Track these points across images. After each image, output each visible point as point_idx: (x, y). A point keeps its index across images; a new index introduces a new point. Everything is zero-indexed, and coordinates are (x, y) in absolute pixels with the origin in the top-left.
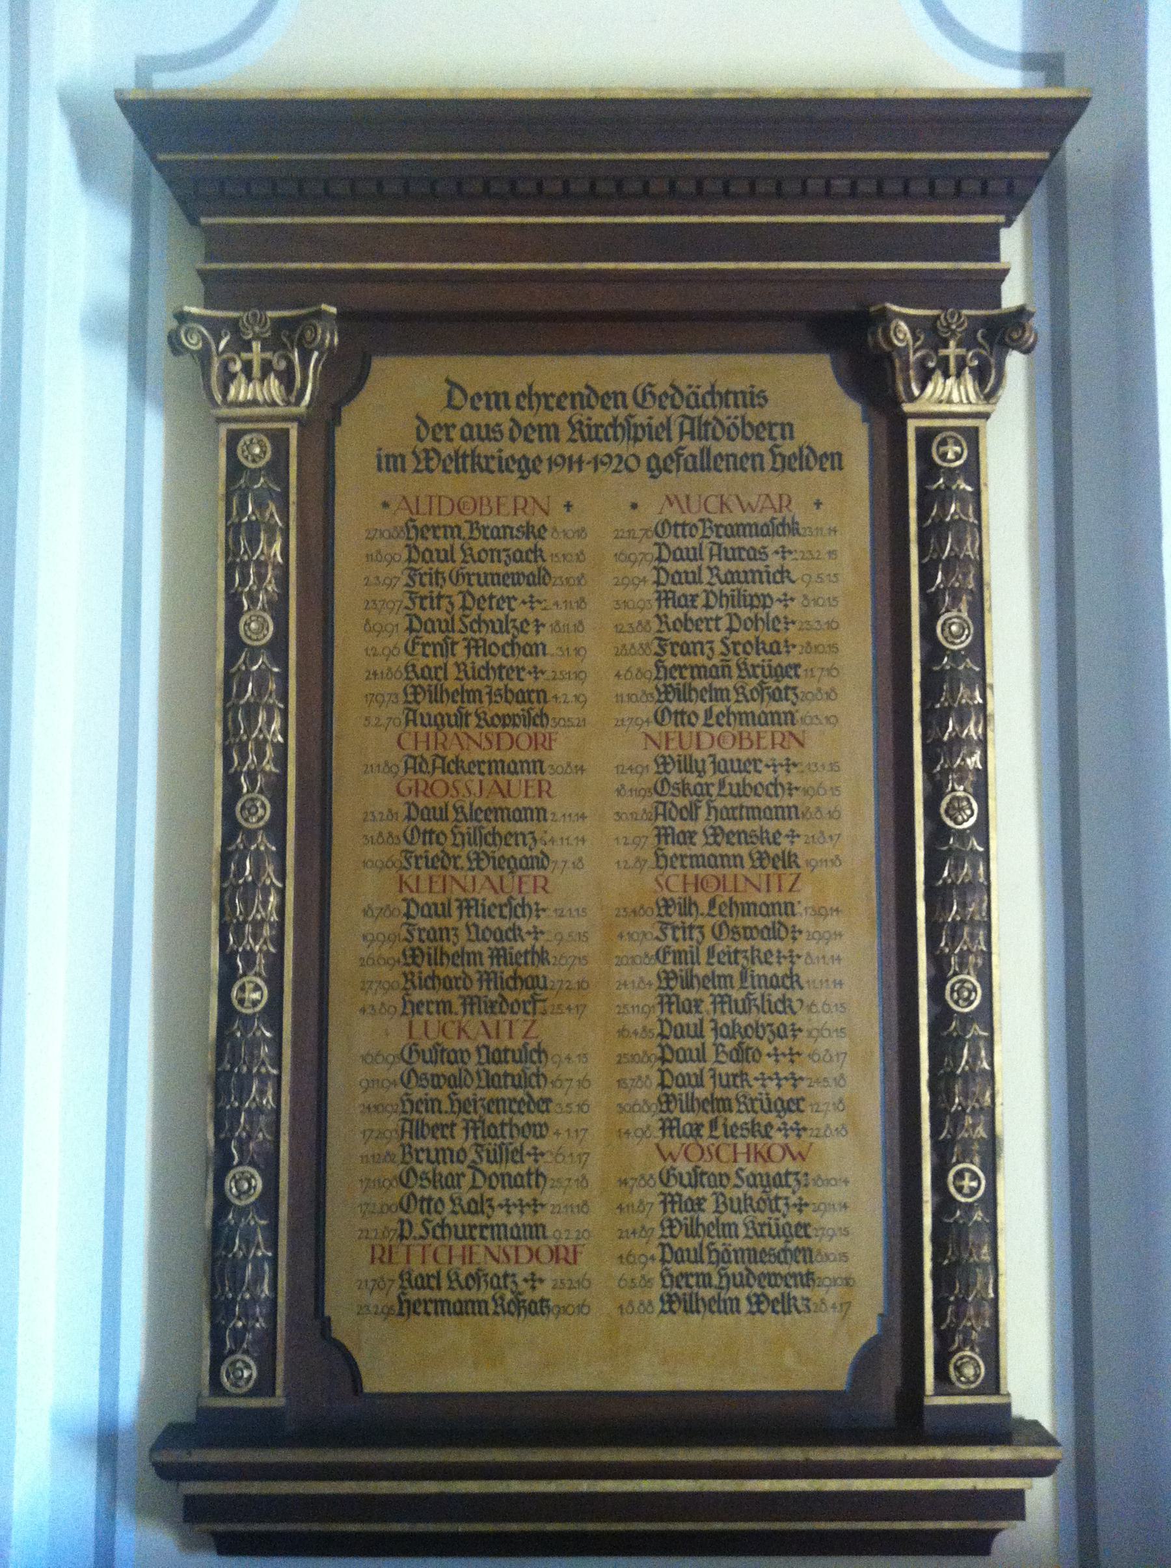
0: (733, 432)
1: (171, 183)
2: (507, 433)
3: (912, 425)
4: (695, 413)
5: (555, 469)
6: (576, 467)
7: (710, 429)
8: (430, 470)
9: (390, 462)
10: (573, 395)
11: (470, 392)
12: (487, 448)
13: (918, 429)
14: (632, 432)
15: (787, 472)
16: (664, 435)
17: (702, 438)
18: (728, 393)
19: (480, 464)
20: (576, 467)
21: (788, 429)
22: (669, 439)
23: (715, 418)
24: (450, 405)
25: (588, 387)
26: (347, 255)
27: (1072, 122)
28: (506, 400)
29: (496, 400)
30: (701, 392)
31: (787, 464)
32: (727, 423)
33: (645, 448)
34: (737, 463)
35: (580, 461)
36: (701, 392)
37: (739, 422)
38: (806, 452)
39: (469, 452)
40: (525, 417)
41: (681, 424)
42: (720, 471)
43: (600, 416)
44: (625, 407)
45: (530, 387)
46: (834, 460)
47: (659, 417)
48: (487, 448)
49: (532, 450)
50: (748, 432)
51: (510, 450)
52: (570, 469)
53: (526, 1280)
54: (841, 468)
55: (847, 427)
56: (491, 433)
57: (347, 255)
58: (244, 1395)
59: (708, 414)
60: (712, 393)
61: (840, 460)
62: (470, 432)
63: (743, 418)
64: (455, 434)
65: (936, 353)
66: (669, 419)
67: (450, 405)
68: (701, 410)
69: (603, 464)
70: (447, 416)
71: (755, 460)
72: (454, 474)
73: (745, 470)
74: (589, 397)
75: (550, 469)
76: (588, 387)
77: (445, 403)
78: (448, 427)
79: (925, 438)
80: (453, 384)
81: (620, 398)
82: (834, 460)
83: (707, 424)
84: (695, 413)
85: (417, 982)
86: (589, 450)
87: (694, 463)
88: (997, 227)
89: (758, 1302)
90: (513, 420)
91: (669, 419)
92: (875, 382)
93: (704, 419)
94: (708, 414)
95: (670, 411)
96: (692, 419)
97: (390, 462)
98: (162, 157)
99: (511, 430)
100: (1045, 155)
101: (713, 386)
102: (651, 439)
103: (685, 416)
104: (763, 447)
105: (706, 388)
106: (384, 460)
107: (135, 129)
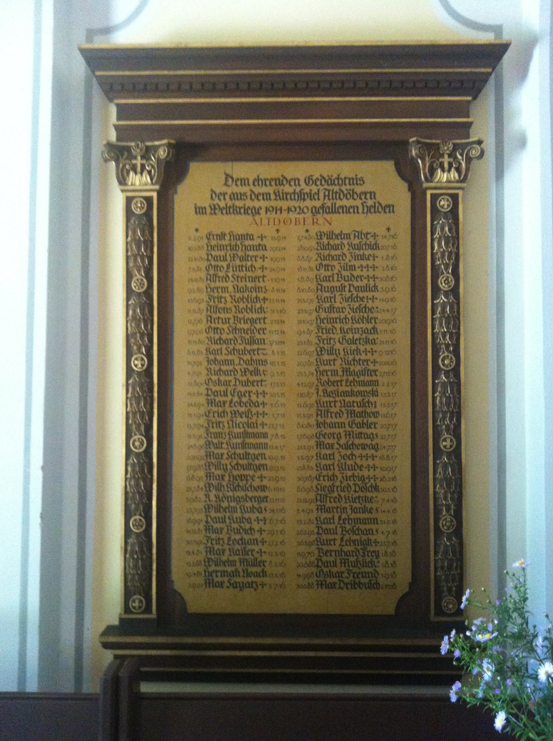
0: (348, 196)
1: (101, 84)
2: (249, 197)
3: (429, 193)
4: (330, 188)
5: (269, 213)
6: (279, 212)
7: (338, 195)
8: (215, 213)
9: (200, 211)
10: (275, 179)
11: (235, 178)
12: (239, 203)
13: (431, 194)
14: (301, 196)
15: (369, 214)
16: (316, 197)
17: (336, 197)
18: (345, 178)
19: (236, 211)
20: (279, 212)
21: (373, 195)
22: (319, 199)
23: (340, 190)
24: (226, 184)
25: (282, 176)
26: (182, 120)
27: (506, 50)
28: (248, 182)
29: (244, 182)
30: (333, 178)
31: (369, 210)
32: (345, 192)
33: (309, 203)
34: (347, 210)
35: (281, 210)
36: (333, 178)
37: (351, 192)
38: (377, 205)
39: (232, 205)
40: (257, 190)
41: (325, 193)
42: (350, 213)
43: (288, 189)
44: (299, 185)
45: (258, 177)
46: (389, 208)
47: (314, 189)
48: (239, 203)
49: (257, 204)
50: (355, 196)
51: (249, 203)
52: (276, 213)
53: (258, 552)
54: (393, 212)
55: (399, 194)
56: (241, 196)
57: (182, 120)
58: (140, 613)
59: (336, 188)
60: (338, 179)
61: (393, 208)
62: (234, 197)
63: (353, 190)
64: (227, 197)
65: (438, 160)
66: (319, 190)
67: (226, 184)
68: (334, 186)
69: (270, 211)
70: (224, 189)
71: (355, 210)
72: (388, 213)
73: (339, 213)
74: (282, 181)
75: (266, 213)
76: (282, 176)
77: (224, 182)
78: (224, 194)
79: (435, 197)
80: (227, 175)
81: (297, 181)
82: (389, 208)
83: (336, 193)
84: (330, 188)
85: (213, 372)
86: (284, 204)
87: (329, 210)
88: (469, 102)
89: (222, 236)
90: (251, 190)
91: (319, 190)
92: (408, 173)
93: (334, 191)
94: (336, 188)
95: (320, 187)
96: (329, 191)
97: (200, 211)
98: (98, 73)
99: (251, 196)
100: (489, 70)
101: (339, 176)
102: (311, 199)
103: (326, 189)
104: (358, 203)
105: (335, 176)
106: (198, 210)
107: (85, 60)
